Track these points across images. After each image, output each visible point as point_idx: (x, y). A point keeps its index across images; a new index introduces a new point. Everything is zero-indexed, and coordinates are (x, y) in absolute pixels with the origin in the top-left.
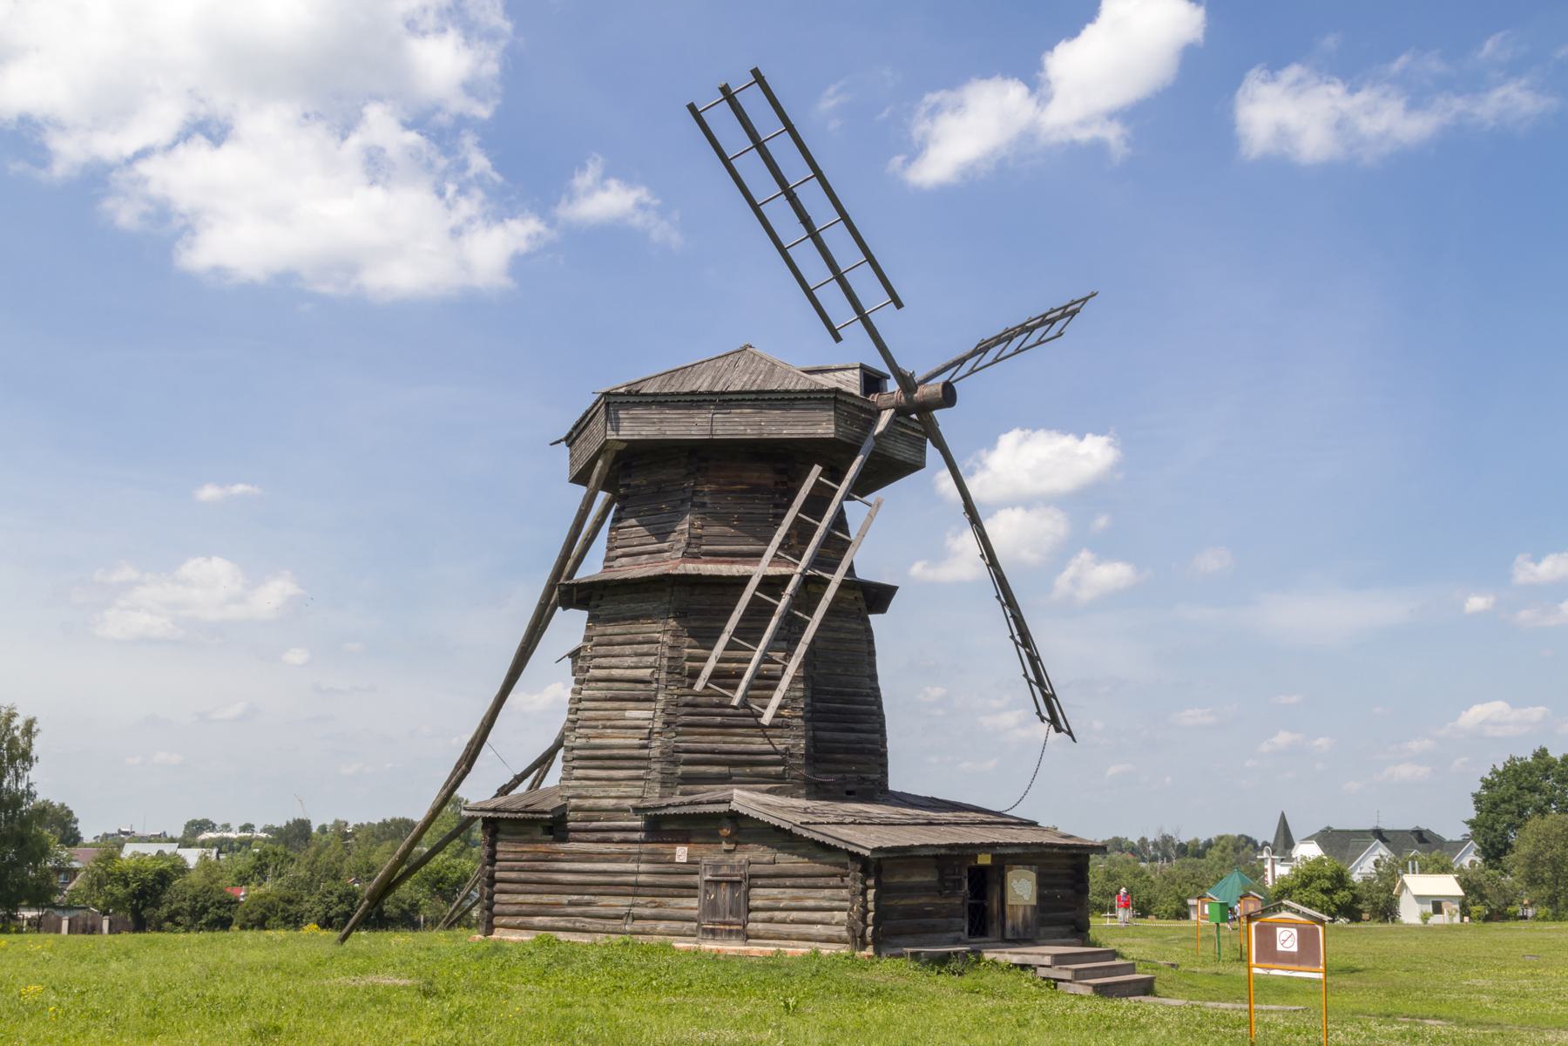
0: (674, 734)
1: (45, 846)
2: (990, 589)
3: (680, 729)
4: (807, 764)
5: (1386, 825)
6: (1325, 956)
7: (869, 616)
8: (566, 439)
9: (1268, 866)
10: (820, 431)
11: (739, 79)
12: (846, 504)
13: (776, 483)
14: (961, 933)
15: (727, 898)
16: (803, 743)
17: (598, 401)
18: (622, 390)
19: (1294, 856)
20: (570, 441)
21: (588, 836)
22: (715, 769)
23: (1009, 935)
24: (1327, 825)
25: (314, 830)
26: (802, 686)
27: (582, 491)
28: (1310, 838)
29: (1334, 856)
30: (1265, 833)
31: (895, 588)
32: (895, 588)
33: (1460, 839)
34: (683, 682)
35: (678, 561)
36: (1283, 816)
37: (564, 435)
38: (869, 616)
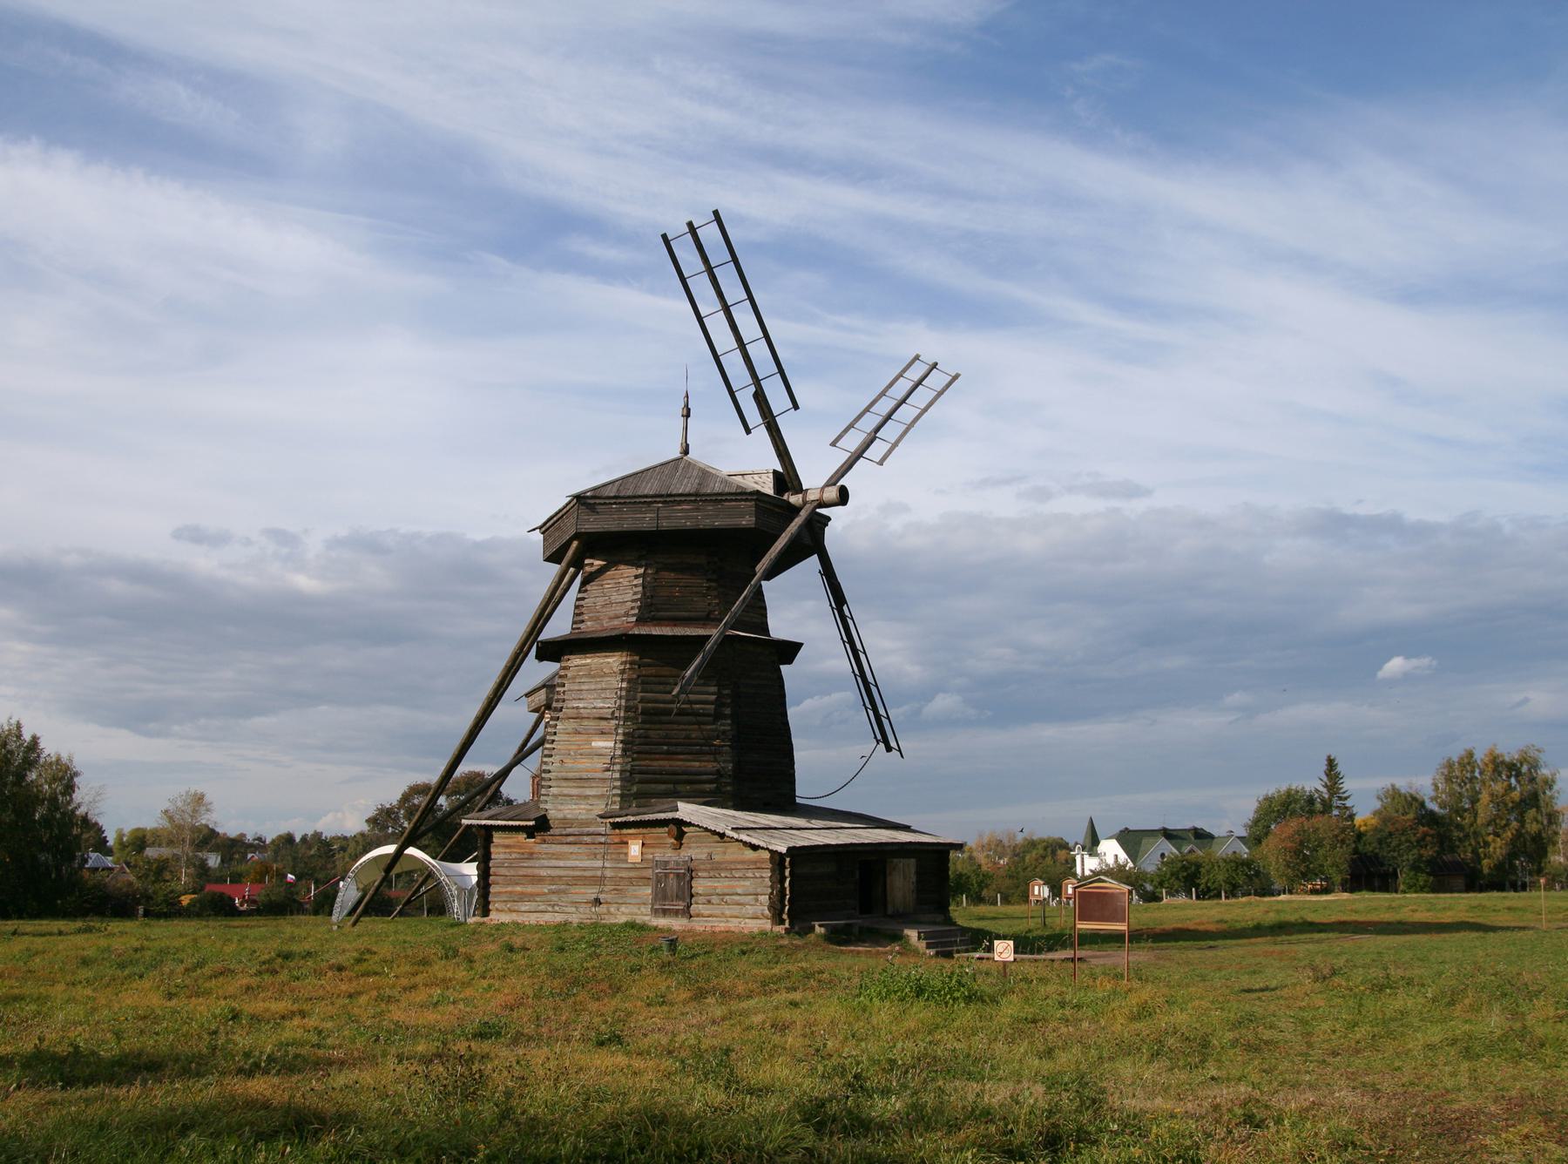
0: (630, 760)
1: (283, 841)
2: (854, 608)
3: (635, 755)
4: (621, 779)
5: (1174, 824)
6: (565, 513)
7: (781, 667)
8: (540, 528)
9: (1078, 859)
10: (744, 523)
11: (677, 227)
12: (763, 583)
13: (709, 563)
14: (853, 911)
15: (675, 887)
16: (730, 766)
17: (570, 502)
18: (588, 494)
19: (1099, 852)
20: (543, 529)
21: (757, 819)
22: (663, 787)
23: (890, 912)
24: (1124, 827)
25: (298, 840)
26: (729, 721)
27: (555, 569)
28: (1111, 838)
29: (627, 709)
30: (1075, 834)
31: (802, 644)
32: (802, 644)
33: (1225, 835)
34: (637, 719)
35: (632, 624)
36: (1091, 818)
37: (540, 523)
38: (781, 667)
